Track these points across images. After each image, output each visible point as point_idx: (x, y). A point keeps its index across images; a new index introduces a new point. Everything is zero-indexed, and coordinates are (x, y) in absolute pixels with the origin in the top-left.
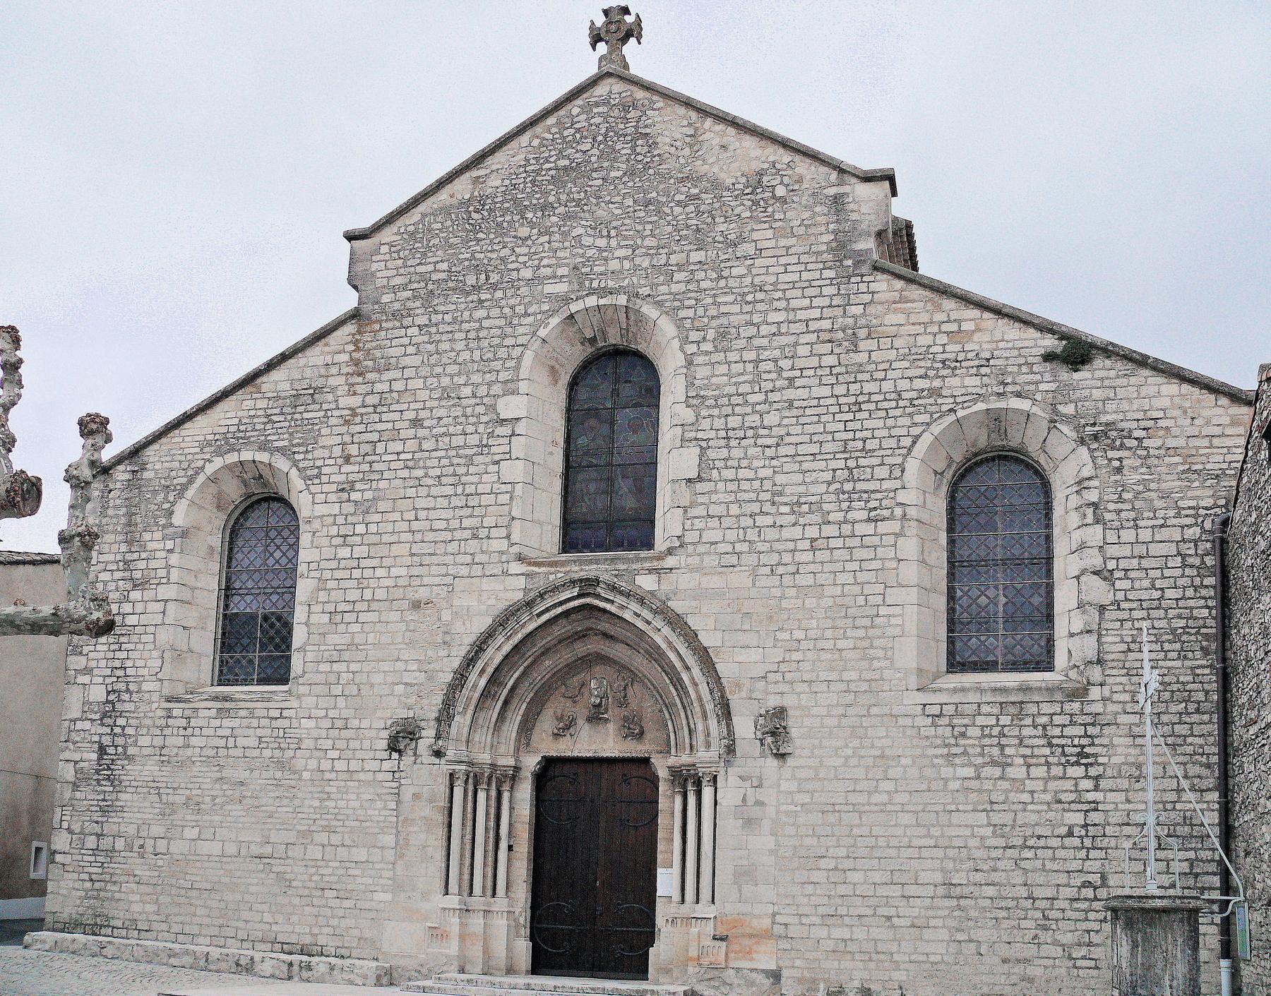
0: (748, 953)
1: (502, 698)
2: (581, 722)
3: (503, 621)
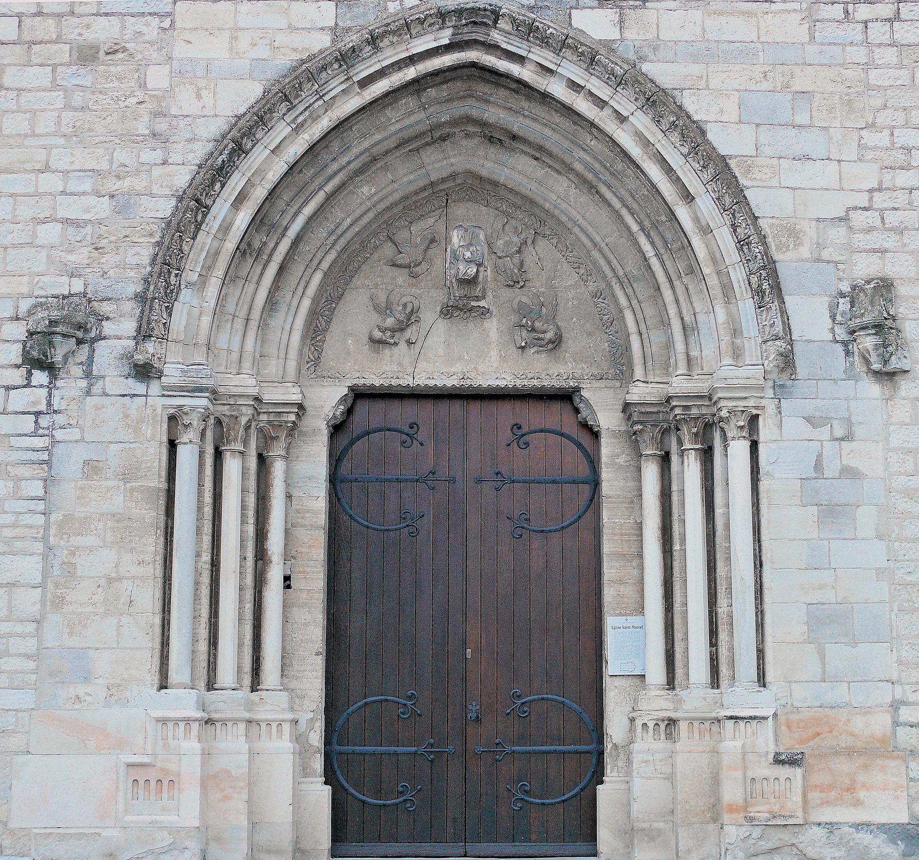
0: (849, 792)
1: (278, 258)
2: (429, 316)
3: (288, 92)
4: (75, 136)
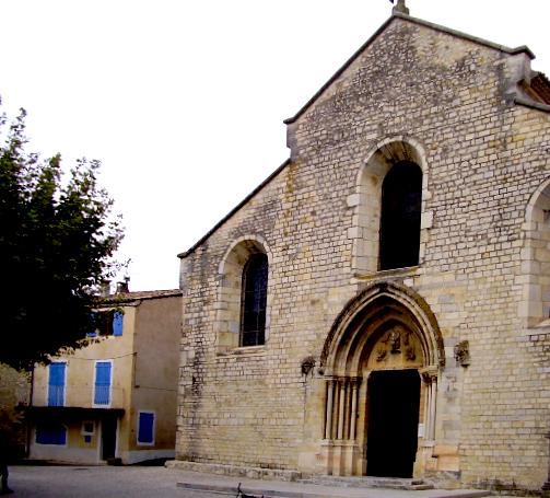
2: (389, 353)
4: (310, 321)
